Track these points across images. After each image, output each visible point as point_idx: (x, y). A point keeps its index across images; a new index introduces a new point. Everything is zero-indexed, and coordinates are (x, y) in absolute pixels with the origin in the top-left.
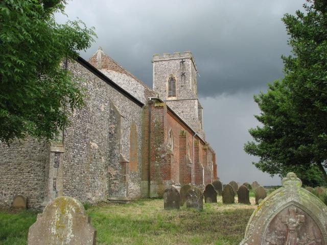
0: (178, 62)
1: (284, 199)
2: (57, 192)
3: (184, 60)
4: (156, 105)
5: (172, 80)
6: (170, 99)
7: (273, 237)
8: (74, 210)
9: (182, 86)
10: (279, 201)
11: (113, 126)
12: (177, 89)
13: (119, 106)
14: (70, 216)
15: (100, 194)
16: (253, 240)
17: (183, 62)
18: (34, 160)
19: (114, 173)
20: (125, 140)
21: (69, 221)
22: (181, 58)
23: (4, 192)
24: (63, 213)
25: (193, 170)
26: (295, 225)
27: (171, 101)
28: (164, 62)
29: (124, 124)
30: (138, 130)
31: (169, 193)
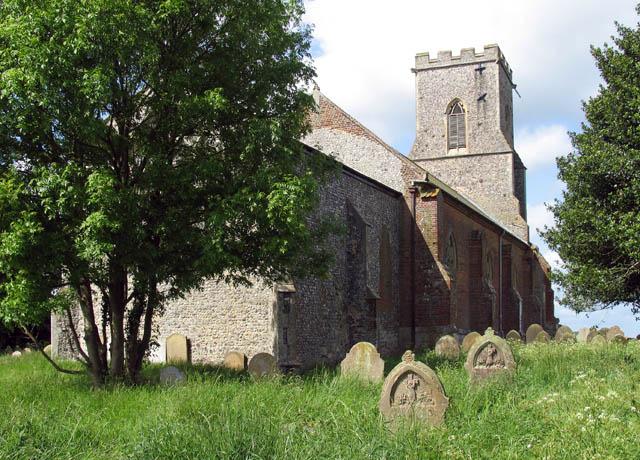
0: (470, 70)
2: (288, 347)
3: (482, 65)
4: (423, 195)
5: (455, 108)
6: (453, 152)
9: (479, 125)
11: (354, 241)
12: (468, 132)
13: (360, 206)
15: (338, 350)
17: (481, 70)
18: (251, 303)
19: (358, 316)
20: (372, 261)
22: (478, 60)
23: (208, 348)
27: (456, 157)
28: (440, 71)
29: (371, 234)
30: (392, 240)
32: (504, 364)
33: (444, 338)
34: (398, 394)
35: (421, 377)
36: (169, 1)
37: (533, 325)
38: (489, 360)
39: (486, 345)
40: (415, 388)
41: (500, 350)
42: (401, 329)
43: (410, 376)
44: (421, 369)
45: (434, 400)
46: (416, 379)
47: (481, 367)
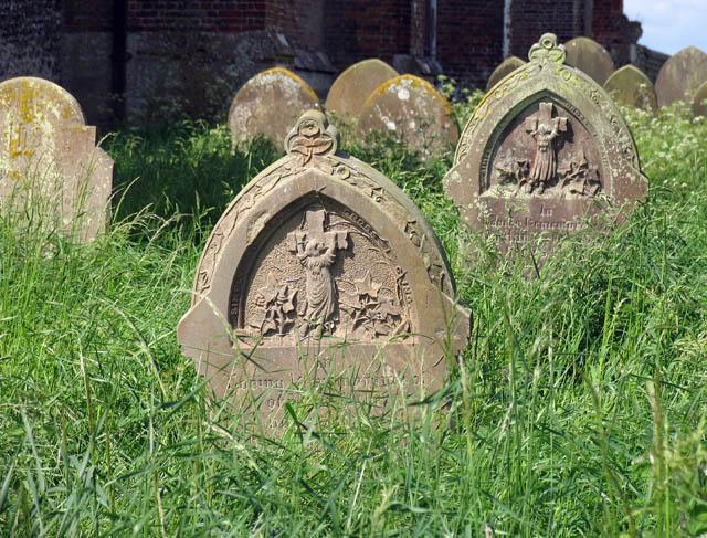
1: (530, 85)
7: (509, 160)
8: (57, 114)
10: (520, 90)
14: (47, 127)
16: (468, 166)
21: (45, 140)
24: (27, 118)
25: (263, 243)
26: (549, 136)
31: (261, 110)
32: (598, 182)
33: (266, 78)
34: (263, 287)
35: (361, 223)
36: (12, 537)
37: (544, 36)
38: (541, 163)
39: (530, 106)
40: (335, 267)
41: (588, 127)
42: (70, 38)
43: (317, 216)
44: (365, 191)
45: (409, 316)
46: (340, 230)
47: (510, 192)
